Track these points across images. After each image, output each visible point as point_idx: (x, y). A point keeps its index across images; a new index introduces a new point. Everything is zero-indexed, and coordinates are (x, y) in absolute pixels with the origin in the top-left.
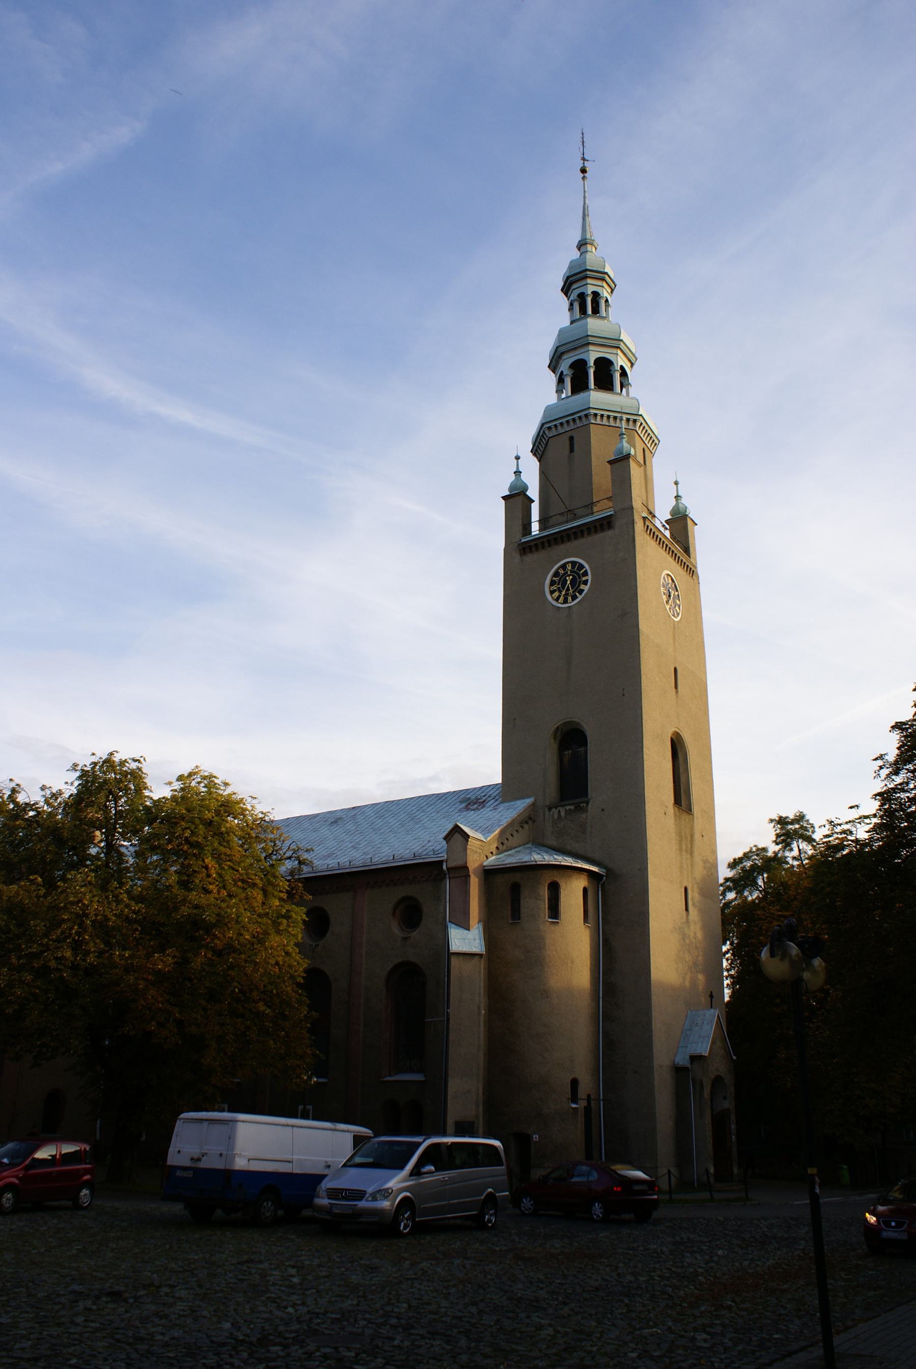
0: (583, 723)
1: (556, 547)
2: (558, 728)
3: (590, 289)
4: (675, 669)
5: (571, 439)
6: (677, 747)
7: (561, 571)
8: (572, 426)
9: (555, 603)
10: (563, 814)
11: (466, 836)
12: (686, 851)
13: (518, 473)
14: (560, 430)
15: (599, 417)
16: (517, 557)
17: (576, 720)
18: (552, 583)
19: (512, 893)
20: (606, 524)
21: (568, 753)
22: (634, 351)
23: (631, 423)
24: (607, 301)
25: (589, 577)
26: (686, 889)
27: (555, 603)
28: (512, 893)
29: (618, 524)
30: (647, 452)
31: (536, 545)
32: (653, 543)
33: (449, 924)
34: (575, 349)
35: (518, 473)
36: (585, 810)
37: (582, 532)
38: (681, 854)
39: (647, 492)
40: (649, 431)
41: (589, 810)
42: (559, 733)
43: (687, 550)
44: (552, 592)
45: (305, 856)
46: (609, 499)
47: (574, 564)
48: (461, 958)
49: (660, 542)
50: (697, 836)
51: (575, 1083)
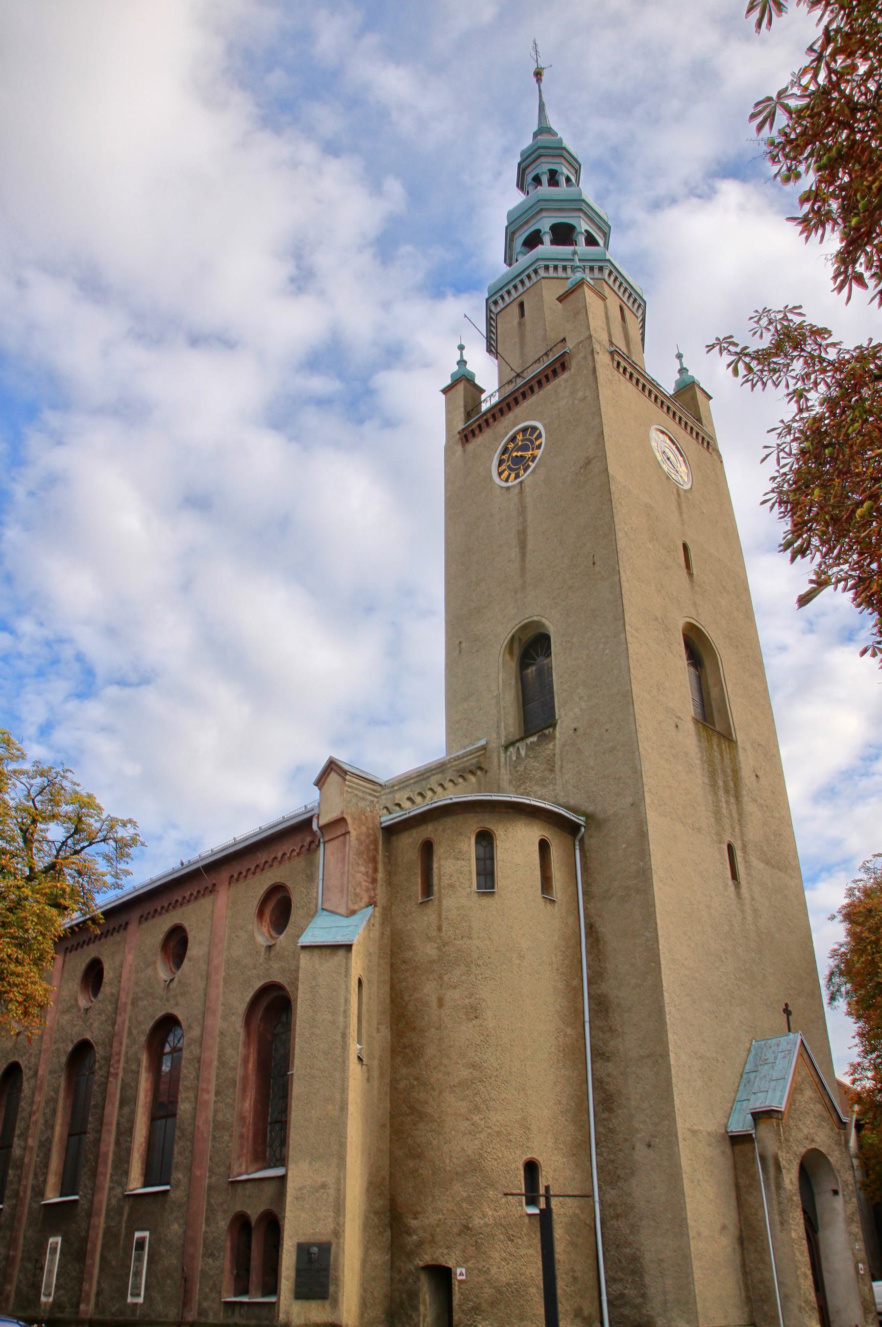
0: (544, 620)
1: (502, 419)
4: (685, 547)
6: (697, 648)
10: (523, 752)
12: (727, 791)
13: (462, 363)
15: (551, 270)
16: (459, 448)
17: (535, 618)
18: (501, 463)
19: (412, 839)
21: (531, 670)
24: (568, 180)
25: (543, 440)
26: (730, 848)
30: (627, 312)
31: (480, 426)
32: (628, 389)
34: (526, 223)
35: (462, 363)
36: (552, 737)
37: (532, 389)
38: (715, 794)
40: (625, 285)
41: (558, 735)
42: (516, 646)
43: (699, 420)
44: (500, 474)
45: (122, 833)
47: (524, 430)
48: (316, 953)
50: (746, 773)
51: (532, 1168)
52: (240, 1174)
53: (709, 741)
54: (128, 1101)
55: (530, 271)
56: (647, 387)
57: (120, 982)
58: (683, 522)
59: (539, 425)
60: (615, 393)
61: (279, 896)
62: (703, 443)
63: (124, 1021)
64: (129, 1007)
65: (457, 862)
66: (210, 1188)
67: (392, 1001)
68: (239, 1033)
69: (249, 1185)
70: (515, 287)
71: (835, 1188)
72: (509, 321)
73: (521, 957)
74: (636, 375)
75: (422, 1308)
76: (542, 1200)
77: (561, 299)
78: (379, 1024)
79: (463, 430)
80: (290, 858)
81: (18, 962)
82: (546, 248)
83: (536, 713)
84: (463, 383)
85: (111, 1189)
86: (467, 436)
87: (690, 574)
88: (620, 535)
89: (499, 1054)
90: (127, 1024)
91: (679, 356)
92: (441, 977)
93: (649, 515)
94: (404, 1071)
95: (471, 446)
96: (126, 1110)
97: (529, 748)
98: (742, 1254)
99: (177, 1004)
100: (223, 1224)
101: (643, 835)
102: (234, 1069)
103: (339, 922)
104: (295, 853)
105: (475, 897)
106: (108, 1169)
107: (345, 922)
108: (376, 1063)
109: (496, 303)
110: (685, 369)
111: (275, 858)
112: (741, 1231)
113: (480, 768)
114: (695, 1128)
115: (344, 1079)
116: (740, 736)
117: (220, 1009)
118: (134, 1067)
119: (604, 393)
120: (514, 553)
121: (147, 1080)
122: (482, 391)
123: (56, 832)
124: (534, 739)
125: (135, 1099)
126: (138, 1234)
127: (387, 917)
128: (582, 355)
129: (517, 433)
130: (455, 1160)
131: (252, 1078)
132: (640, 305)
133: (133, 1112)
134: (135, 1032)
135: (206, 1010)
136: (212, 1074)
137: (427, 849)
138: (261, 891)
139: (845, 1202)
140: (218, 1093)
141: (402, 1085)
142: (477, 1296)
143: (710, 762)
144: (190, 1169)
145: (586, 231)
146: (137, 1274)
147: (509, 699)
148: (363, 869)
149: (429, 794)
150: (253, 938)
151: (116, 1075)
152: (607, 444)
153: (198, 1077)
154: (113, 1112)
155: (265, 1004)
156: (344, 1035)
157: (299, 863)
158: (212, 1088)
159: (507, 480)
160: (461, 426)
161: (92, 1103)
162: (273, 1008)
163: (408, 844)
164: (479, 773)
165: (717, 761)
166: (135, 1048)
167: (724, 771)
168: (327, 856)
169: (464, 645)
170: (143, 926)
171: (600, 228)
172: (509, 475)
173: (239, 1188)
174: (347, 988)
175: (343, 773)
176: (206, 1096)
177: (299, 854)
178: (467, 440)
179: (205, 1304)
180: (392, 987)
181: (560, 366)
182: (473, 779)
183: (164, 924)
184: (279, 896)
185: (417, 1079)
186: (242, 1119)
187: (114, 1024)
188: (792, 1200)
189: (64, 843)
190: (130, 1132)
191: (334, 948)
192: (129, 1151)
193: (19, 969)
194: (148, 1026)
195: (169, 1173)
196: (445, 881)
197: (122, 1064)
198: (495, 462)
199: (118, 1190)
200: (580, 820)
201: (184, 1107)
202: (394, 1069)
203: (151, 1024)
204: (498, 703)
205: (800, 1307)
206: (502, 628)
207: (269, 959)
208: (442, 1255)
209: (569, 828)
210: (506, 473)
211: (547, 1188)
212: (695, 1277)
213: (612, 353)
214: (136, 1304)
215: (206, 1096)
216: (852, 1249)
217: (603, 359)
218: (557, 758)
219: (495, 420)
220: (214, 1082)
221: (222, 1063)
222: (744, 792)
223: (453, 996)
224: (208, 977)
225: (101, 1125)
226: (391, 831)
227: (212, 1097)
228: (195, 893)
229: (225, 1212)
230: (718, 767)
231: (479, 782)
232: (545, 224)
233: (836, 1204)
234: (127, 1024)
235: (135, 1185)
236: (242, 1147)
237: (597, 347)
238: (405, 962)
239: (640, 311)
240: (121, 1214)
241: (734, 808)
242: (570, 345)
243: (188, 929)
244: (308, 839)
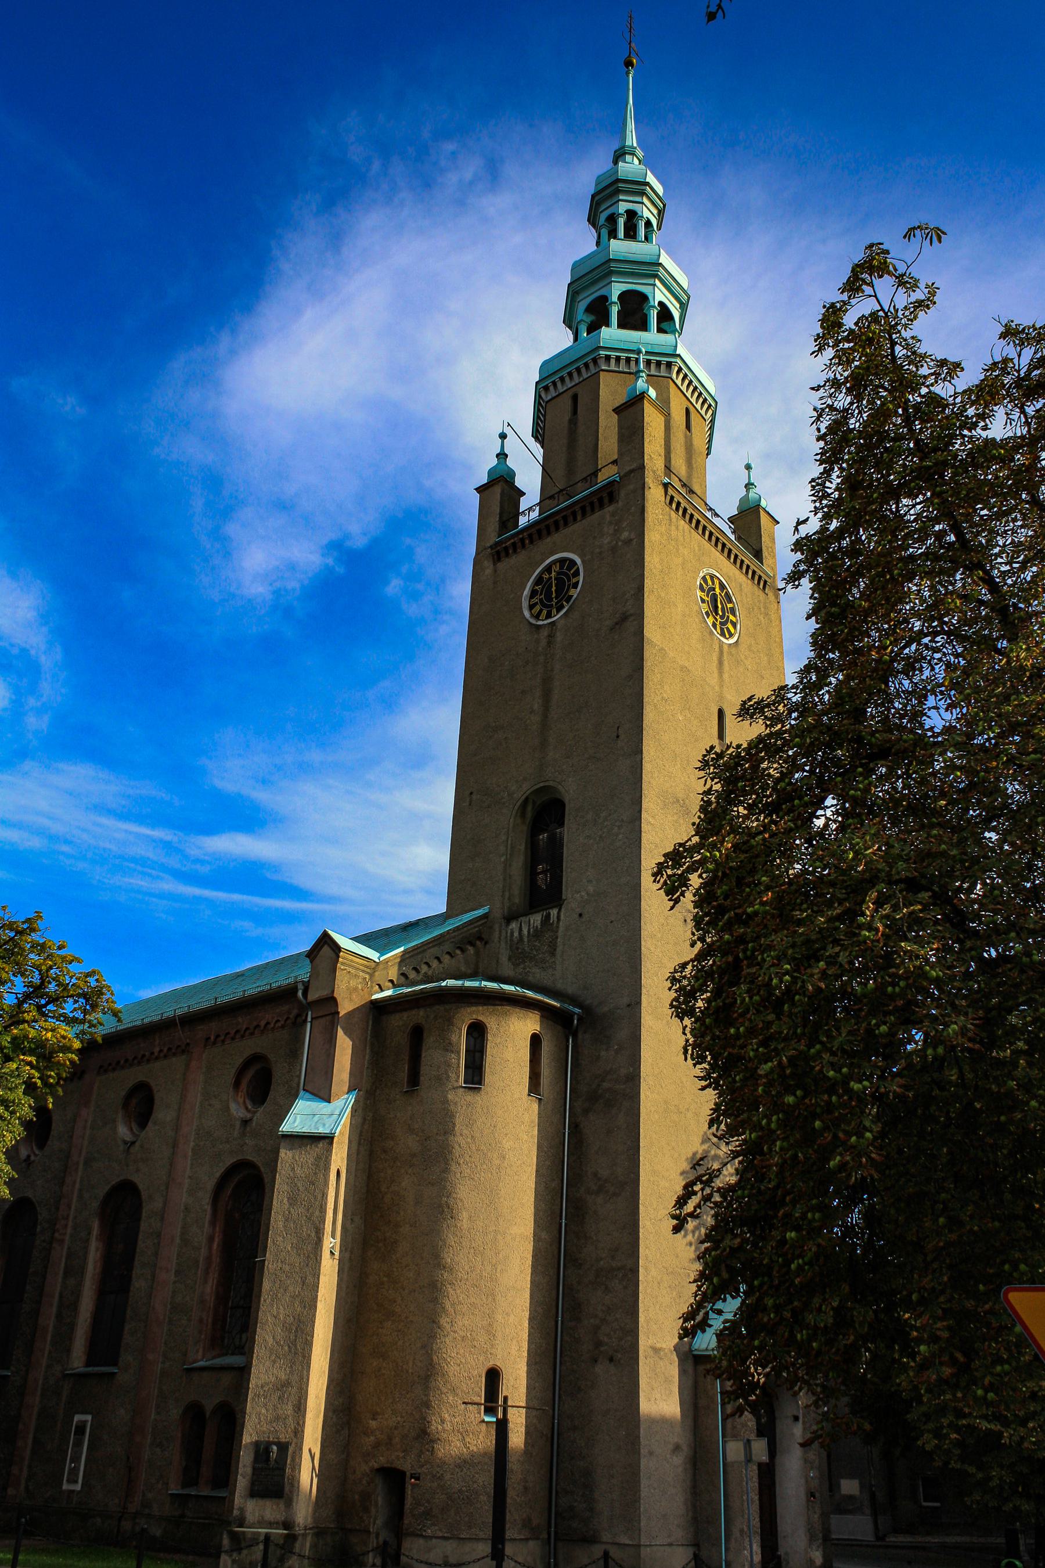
2: (527, 799)
3: (623, 207)
5: (575, 398)
7: (546, 576)
8: (576, 379)
11: (337, 948)
13: (502, 456)
14: (561, 388)
15: (613, 362)
16: (488, 564)
17: (551, 783)
18: (533, 593)
20: (609, 494)
21: (544, 836)
22: (685, 287)
23: (663, 367)
24: (648, 224)
28: (411, 1045)
30: (694, 415)
31: (514, 545)
33: (302, 1093)
35: (502, 456)
42: (529, 808)
43: (758, 554)
44: (531, 607)
46: (615, 462)
47: (562, 561)
49: (724, 549)
51: (493, 1376)
52: (195, 1361)
54: (74, 1270)
57: (71, 1137)
58: (721, 686)
59: (578, 561)
62: (759, 583)
63: (75, 1182)
68: (206, 1211)
71: (796, 1413)
75: (373, 1510)
76: (500, 1410)
78: (353, 1214)
79: (497, 544)
80: (273, 1028)
84: (500, 487)
89: (471, 1257)
90: (77, 1186)
93: (683, 680)
95: (503, 565)
98: (694, 1475)
99: (138, 1170)
100: (175, 1412)
104: (279, 1024)
110: (753, 484)
111: (258, 1026)
112: (695, 1452)
113: (480, 939)
114: (658, 1345)
119: (653, 536)
121: (97, 1249)
129: (554, 562)
130: (419, 1364)
131: (216, 1260)
132: (710, 406)
137: (417, 1035)
138: (239, 1061)
139: (804, 1429)
140: (178, 1273)
142: (428, 1502)
145: (661, 304)
146: (76, 1459)
150: (228, 1108)
151: (62, 1241)
155: (232, 1186)
159: (537, 617)
160: (493, 538)
161: (31, 1270)
164: (478, 943)
172: (541, 611)
177: (283, 1027)
178: (499, 559)
179: (150, 1495)
180: (370, 1176)
182: (471, 950)
188: (747, 1425)
190: (74, 1306)
192: (72, 1327)
194: (102, 1191)
197: (69, 1230)
198: (527, 592)
201: (139, 1284)
203: (107, 1188)
205: (742, 1531)
208: (398, 1457)
210: (538, 608)
211: (506, 1398)
212: (643, 1495)
213: (666, 486)
214: (73, 1491)
216: (807, 1477)
219: (531, 542)
224: (175, 1145)
228: (165, 1050)
231: (477, 953)
233: (795, 1431)
234: (77, 1186)
238: (385, 1151)
239: (710, 412)
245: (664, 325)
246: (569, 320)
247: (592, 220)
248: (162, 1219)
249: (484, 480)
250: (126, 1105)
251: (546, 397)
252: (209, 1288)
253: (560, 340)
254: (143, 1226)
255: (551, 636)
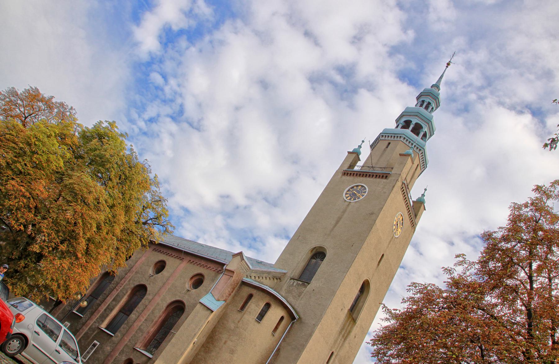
4: (383, 255)
6: (365, 287)
9: (345, 198)
10: (295, 284)
12: (343, 336)
13: (360, 147)
14: (386, 138)
16: (340, 175)
18: (349, 190)
19: (248, 292)
24: (433, 108)
25: (366, 194)
26: (332, 353)
27: (345, 198)
29: (390, 178)
30: (419, 167)
33: (210, 293)
34: (410, 115)
35: (360, 147)
36: (306, 287)
39: (411, 179)
42: (315, 250)
43: (416, 216)
44: (346, 194)
45: (170, 229)
47: (362, 186)
48: (203, 306)
53: (348, 319)
54: (116, 300)
55: (399, 135)
56: (406, 198)
58: (388, 247)
59: (367, 189)
60: (396, 196)
61: (200, 277)
64: (134, 273)
65: (255, 306)
66: (126, 345)
67: (212, 331)
69: (139, 353)
70: (391, 136)
72: (382, 145)
73: (255, 346)
74: (405, 194)
77: (400, 155)
81: (123, 253)
82: (408, 132)
83: (306, 276)
84: (355, 154)
85: (95, 322)
86: (345, 173)
87: (378, 265)
88: (366, 243)
91: (426, 190)
92: (230, 335)
94: (202, 353)
96: (114, 303)
97: (298, 284)
100: (124, 358)
101: (311, 335)
102: (155, 317)
103: (212, 300)
105: (254, 320)
106: (97, 315)
107: (215, 302)
108: (196, 346)
109: (383, 136)
115: (187, 347)
116: (358, 322)
117: (162, 296)
118: (124, 292)
120: (333, 222)
122: (359, 160)
123: (152, 214)
124: (301, 283)
125: (119, 302)
126: (95, 341)
127: (226, 307)
128: (394, 178)
131: (158, 323)
133: (116, 305)
134: (131, 282)
135: (157, 294)
136: (147, 313)
137: (250, 296)
138: (196, 272)
140: (146, 320)
141: (199, 357)
143: (344, 325)
144: (124, 335)
145: (425, 132)
146: (88, 353)
147: (302, 265)
148: (229, 290)
149: (261, 278)
151: (117, 290)
152: (381, 212)
153: (143, 311)
154: (109, 300)
156: (195, 335)
157: (213, 273)
158: (145, 317)
162: (177, 309)
163: (246, 291)
165: (346, 326)
166: (128, 287)
167: (346, 330)
168: (222, 279)
169: (300, 237)
170: (154, 252)
171: (430, 132)
173: (135, 352)
174: (205, 322)
175: (242, 259)
176: (141, 318)
180: (214, 328)
181: (385, 176)
182: (276, 281)
183: (162, 257)
184: (200, 277)
185: (204, 358)
186: (148, 333)
187: (126, 274)
189: (151, 219)
190: (112, 310)
191: (208, 309)
192: (108, 315)
193: (122, 255)
194: (137, 283)
195: (116, 332)
196: (249, 310)
197: (121, 288)
198: (347, 189)
199: (97, 324)
200: (297, 317)
201: (133, 316)
202: (200, 351)
203: (138, 284)
204: (298, 264)
206: (315, 242)
207: (186, 294)
209: (293, 318)
213: (403, 183)
215: (141, 318)
217: (399, 184)
218: (303, 294)
220: (147, 316)
221: (153, 312)
222: (348, 339)
223: (230, 343)
224: (164, 284)
225: (104, 301)
226: (244, 283)
227: (143, 320)
229: (126, 355)
230: (345, 328)
231: (277, 283)
232: (414, 121)
235: (103, 326)
236: (143, 340)
237: (400, 179)
240: (94, 332)
241: (342, 342)
242: (393, 172)
243: (167, 265)
244: (220, 269)
245: (423, 138)
246: (397, 121)
247: (418, 98)
248: (150, 302)
249: (351, 151)
250: (156, 264)
251: (381, 138)
252: (152, 330)
253: (392, 125)
254: (143, 301)
255: (348, 205)
